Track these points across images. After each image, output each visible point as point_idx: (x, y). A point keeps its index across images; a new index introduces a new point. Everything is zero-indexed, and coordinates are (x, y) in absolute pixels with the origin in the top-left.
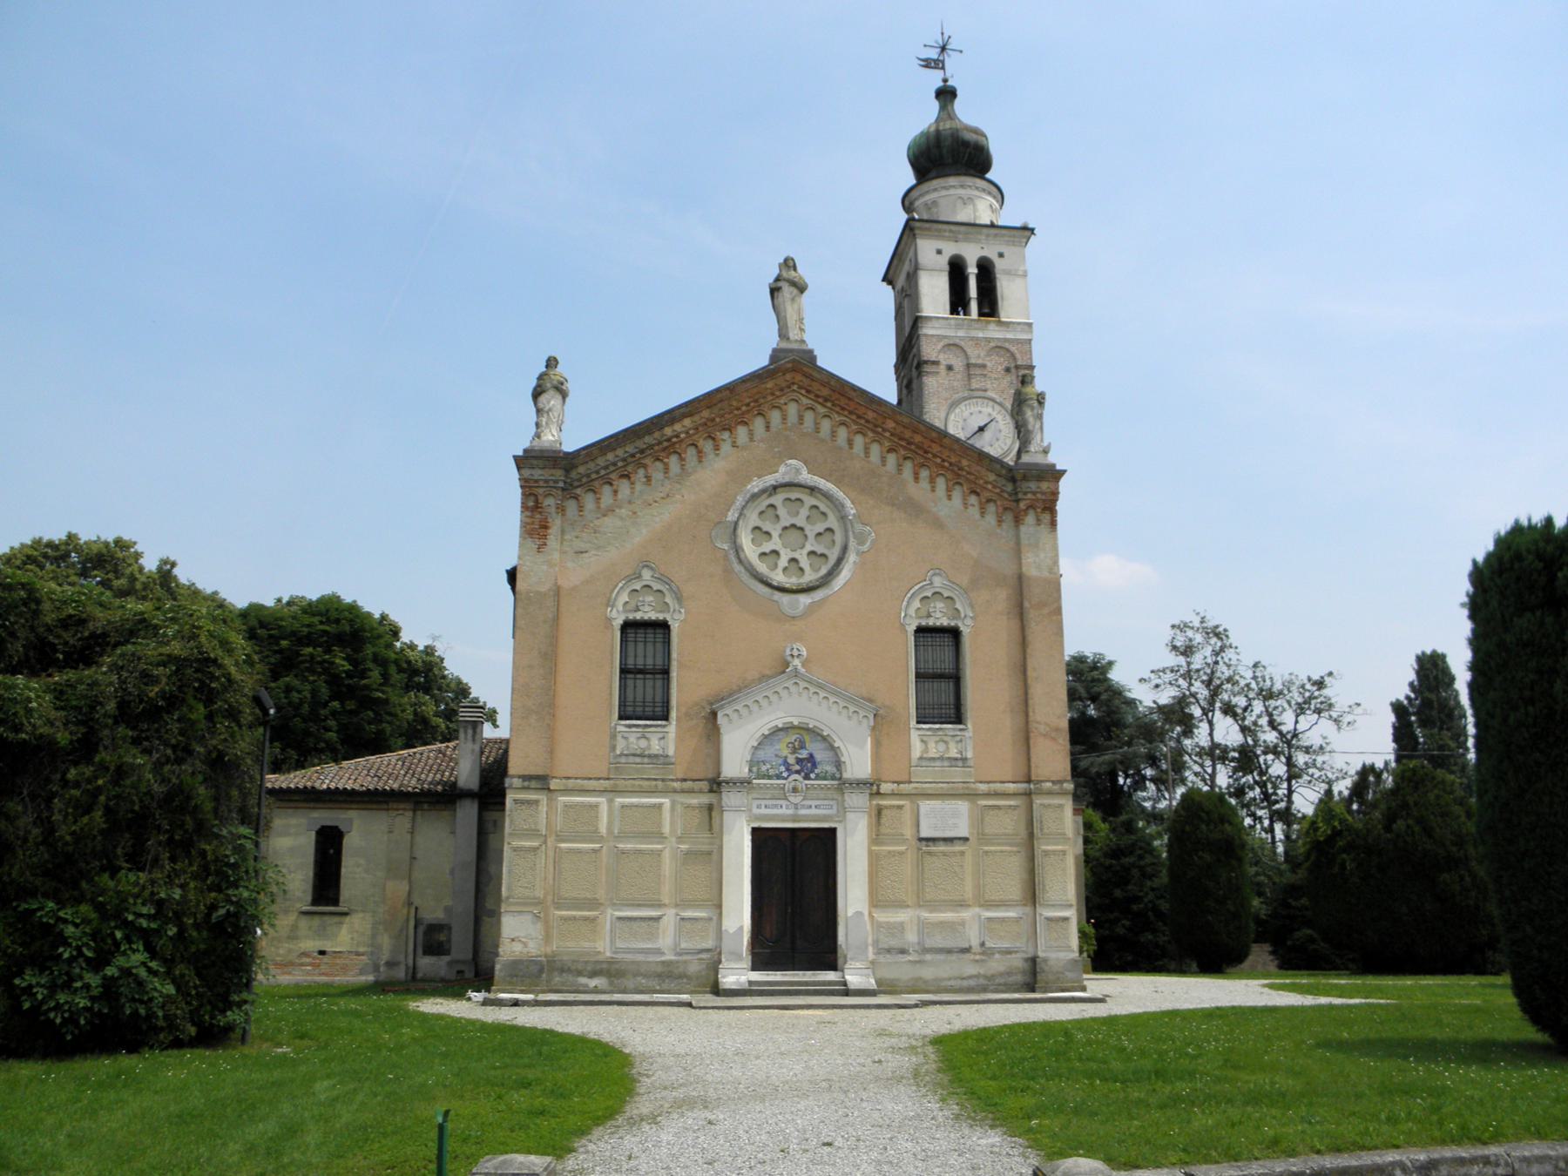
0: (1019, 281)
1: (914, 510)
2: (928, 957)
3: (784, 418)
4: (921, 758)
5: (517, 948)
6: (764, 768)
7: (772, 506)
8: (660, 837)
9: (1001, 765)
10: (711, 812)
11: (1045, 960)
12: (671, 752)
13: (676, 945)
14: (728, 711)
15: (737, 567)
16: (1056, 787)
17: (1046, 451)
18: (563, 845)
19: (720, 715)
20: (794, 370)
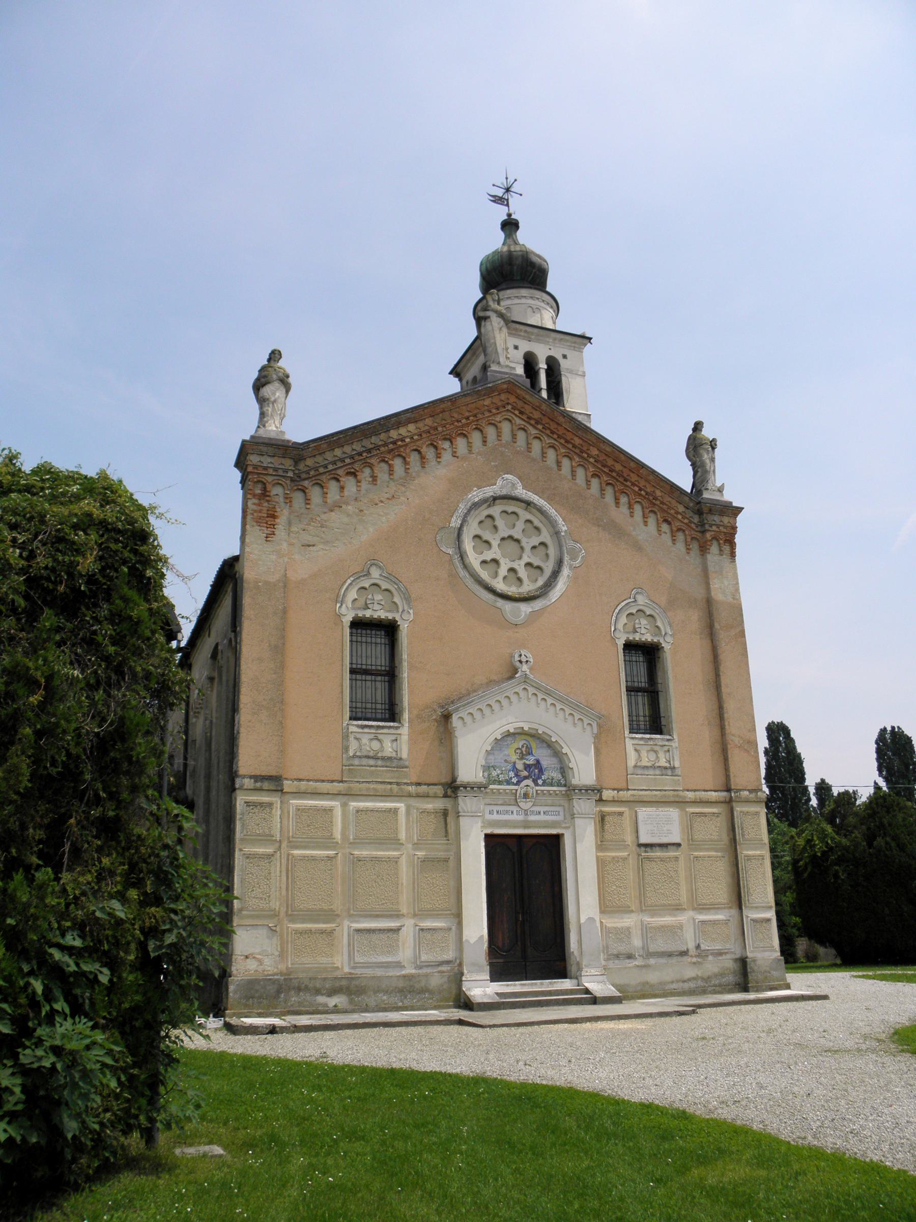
0: (579, 379)
1: (617, 532)
2: (652, 961)
3: (499, 435)
4: (635, 766)
5: (252, 965)
6: (494, 773)
7: (490, 516)
8: (395, 842)
9: (702, 774)
10: (447, 820)
11: (754, 961)
12: (404, 755)
13: (416, 957)
14: (463, 713)
15: (462, 573)
16: (753, 795)
17: (720, 490)
18: (296, 852)
19: (455, 718)
20: (508, 391)
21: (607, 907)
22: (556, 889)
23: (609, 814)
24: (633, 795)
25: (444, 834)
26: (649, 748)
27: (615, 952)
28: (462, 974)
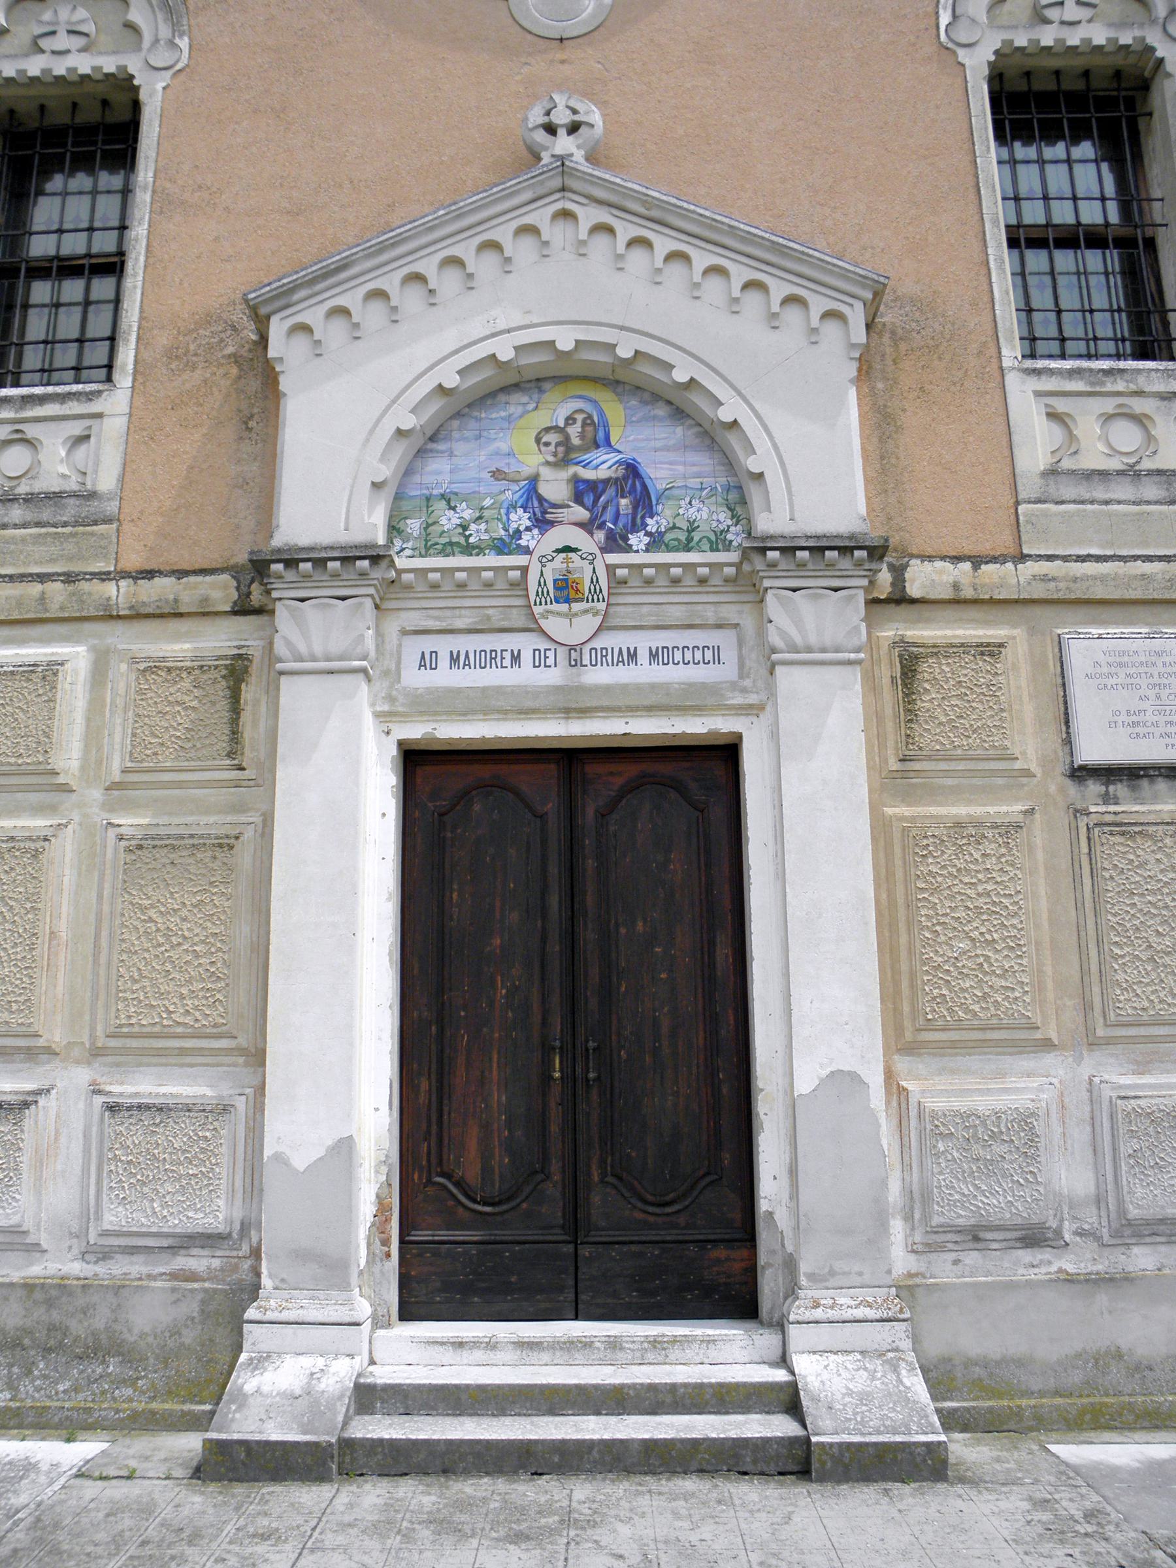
2: (1142, 1259)
4: (1052, 473)
6: (448, 521)
8: (47, 785)
12: (106, 481)
13: (89, 1213)
19: (277, 329)
21: (929, 1025)
22: (723, 953)
23: (937, 651)
24: (1045, 579)
25: (223, 745)
26: (1109, 405)
27: (963, 1218)
28: (253, 1291)
